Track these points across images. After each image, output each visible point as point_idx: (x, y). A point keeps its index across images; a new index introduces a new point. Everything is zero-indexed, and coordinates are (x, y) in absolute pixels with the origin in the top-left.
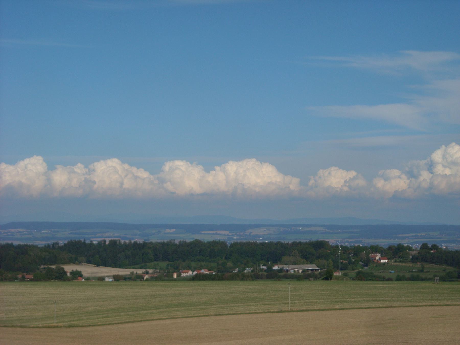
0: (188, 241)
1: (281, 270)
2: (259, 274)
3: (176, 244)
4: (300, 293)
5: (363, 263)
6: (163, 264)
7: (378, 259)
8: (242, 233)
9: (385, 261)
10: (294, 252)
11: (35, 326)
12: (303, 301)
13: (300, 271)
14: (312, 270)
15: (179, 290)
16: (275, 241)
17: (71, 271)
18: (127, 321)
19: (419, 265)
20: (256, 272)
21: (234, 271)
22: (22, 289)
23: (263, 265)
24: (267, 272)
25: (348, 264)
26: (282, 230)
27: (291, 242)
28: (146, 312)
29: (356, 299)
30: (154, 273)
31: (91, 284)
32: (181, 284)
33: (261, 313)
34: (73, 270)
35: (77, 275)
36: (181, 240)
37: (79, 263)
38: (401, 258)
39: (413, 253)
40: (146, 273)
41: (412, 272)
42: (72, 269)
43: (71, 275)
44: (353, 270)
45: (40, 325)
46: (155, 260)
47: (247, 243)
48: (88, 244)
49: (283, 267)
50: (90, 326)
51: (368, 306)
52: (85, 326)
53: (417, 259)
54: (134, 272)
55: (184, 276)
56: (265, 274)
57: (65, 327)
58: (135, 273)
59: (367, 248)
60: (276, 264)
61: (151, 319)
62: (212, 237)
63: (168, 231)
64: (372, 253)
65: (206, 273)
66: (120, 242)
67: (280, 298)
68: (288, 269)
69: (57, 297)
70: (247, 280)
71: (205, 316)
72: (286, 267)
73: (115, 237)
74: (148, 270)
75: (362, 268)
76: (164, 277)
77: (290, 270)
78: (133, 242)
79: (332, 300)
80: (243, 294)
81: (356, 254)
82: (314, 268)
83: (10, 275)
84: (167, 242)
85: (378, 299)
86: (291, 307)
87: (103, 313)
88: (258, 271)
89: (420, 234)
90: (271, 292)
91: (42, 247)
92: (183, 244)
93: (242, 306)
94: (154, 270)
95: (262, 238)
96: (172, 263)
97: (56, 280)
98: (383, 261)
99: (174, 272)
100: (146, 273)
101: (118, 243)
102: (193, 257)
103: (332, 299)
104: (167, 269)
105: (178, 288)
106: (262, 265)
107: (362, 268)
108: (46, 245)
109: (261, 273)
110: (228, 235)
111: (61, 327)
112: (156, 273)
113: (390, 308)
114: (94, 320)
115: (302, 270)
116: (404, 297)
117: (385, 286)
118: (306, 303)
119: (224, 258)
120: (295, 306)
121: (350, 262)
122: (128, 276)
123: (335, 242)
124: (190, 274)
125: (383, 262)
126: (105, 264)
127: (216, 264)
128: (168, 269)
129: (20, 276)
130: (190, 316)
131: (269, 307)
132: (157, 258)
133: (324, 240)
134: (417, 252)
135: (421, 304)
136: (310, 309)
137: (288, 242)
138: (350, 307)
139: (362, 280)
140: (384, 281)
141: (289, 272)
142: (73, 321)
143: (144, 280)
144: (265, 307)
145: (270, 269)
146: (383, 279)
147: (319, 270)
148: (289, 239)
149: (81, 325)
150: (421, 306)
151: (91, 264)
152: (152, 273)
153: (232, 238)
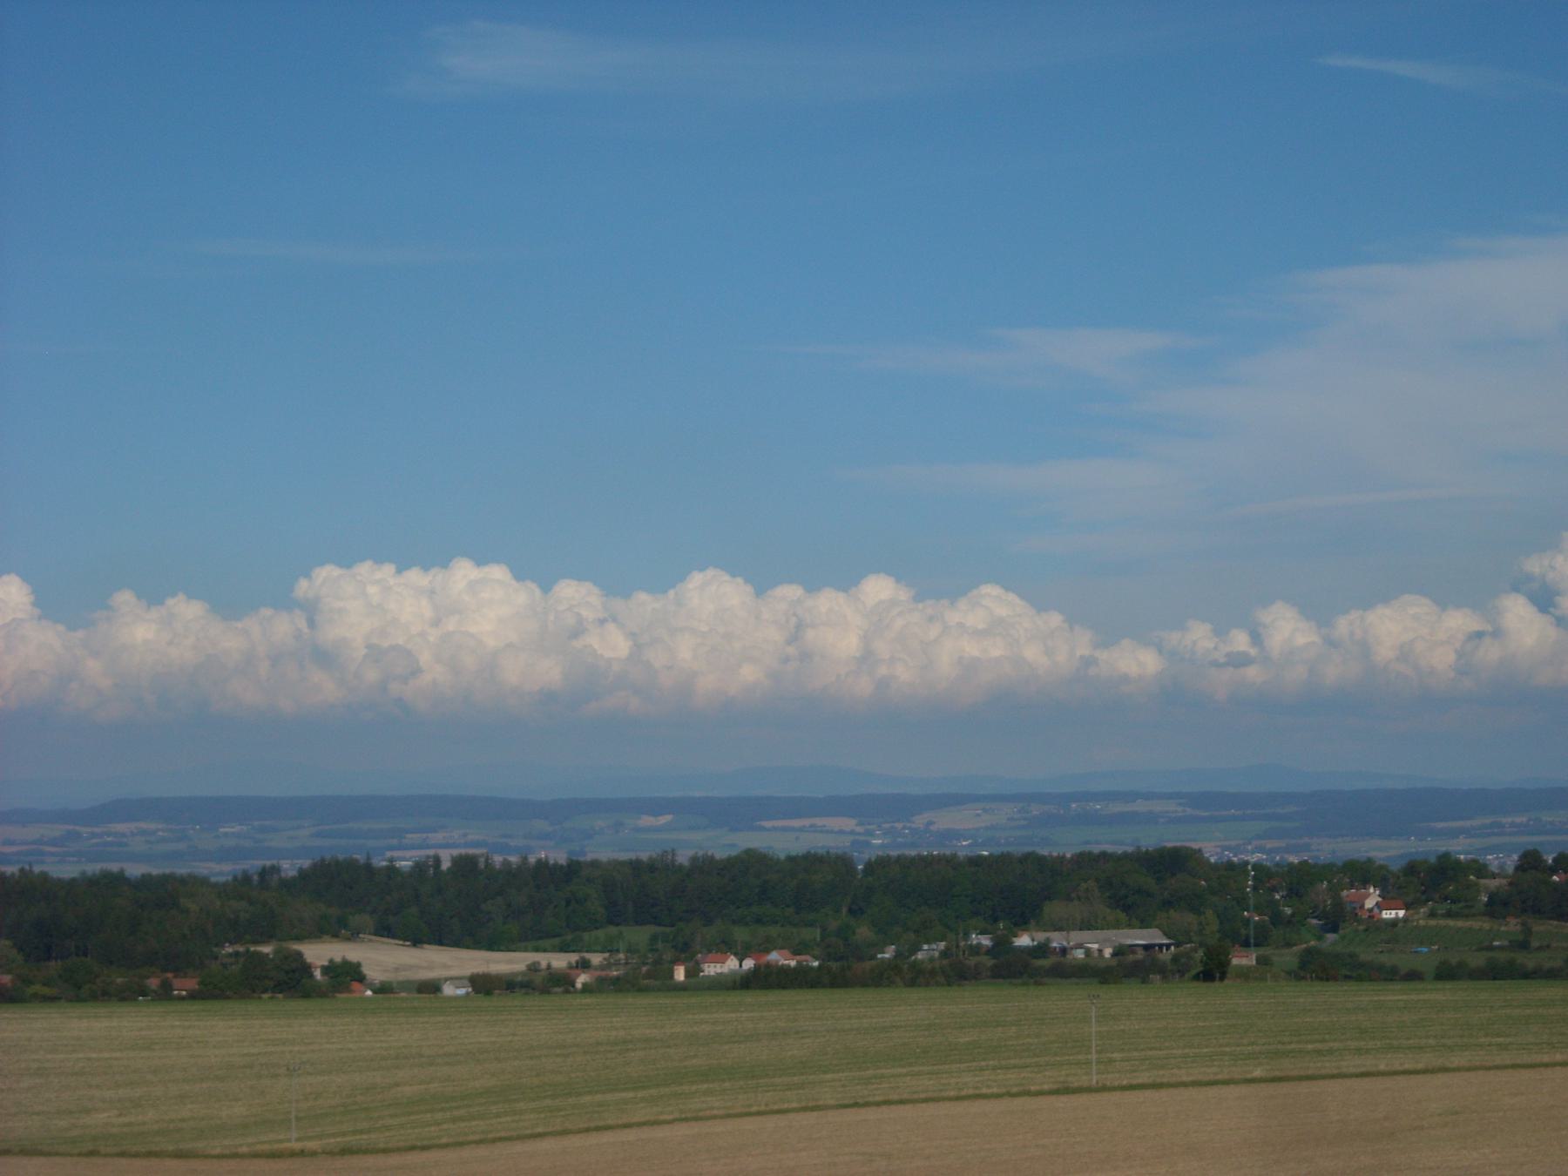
0: (720, 854)
1: (1042, 950)
2: (967, 961)
3: (681, 866)
4: (1122, 1027)
5: (1320, 920)
6: (640, 935)
7: (1371, 906)
8: (899, 825)
9: (1397, 913)
10: (1084, 885)
11: (227, 1152)
12: (1136, 1054)
13: (1108, 952)
14: (1147, 947)
15: (707, 1022)
16: (1018, 850)
17: (326, 963)
18: (540, 1130)
19: (1512, 925)
20: (957, 955)
21: (879, 956)
22: (173, 1027)
23: (978, 931)
24: (994, 958)
25: (1271, 926)
26: (1035, 813)
27: (1074, 852)
28: (599, 1097)
29: (1319, 1046)
30: (606, 966)
31: (405, 1005)
32: (712, 1000)
33: (998, 1096)
34: (331, 961)
35: (346, 976)
36: (696, 853)
37: (353, 936)
38: (1451, 903)
39: (1493, 884)
40: (580, 965)
41: (1491, 948)
42: (329, 957)
43: (326, 978)
44: (1289, 945)
45: (244, 1149)
46: (611, 922)
47: (921, 858)
48: (381, 869)
49: (1048, 940)
50: (412, 1148)
51: (1363, 1070)
52: (398, 1150)
53: (1505, 904)
54: (539, 963)
55: (712, 973)
56: (989, 962)
57: (330, 1153)
58: (544, 965)
59: (1335, 869)
60: (1023, 930)
61: (620, 1122)
62: (797, 838)
63: (647, 821)
64: (1352, 887)
65: (787, 962)
66: (490, 861)
67: (1056, 1045)
68: (1065, 943)
69: (291, 1052)
70: (927, 985)
71: (805, 1109)
72: (1057, 940)
73: (466, 845)
74: (587, 956)
75: (1320, 938)
76: (643, 979)
77: (1072, 948)
78: (532, 860)
79: (1238, 1049)
80: (926, 1033)
81: (1294, 892)
82: (1153, 942)
83: (119, 980)
84: (650, 858)
85: (1395, 1043)
86: (1098, 1073)
87: (454, 1104)
88: (964, 951)
89: (1510, 820)
90: (1024, 1025)
91: (225, 884)
92: (704, 866)
93: (928, 1074)
94: (607, 955)
95: (970, 841)
96: (668, 930)
97: (280, 996)
98: (1391, 914)
99: (676, 961)
100: (580, 965)
101: (482, 865)
102: (739, 907)
103: (1238, 1046)
104: (652, 950)
105: (702, 1016)
106: (977, 934)
107: (1320, 938)
108: (239, 877)
109: (973, 961)
110: (852, 832)
111: (313, 1154)
112: (615, 964)
113: (1440, 1075)
114: (426, 1129)
115: (1114, 948)
116: (1486, 1035)
117: (1414, 997)
118: (1147, 1062)
119: (844, 910)
120: (1113, 1072)
121: (1277, 919)
122: (520, 979)
123: (1219, 850)
124: (732, 967)
125: (1388, 916)
126: (440, 936)
127: (818, 931)
128: (657, 950)
129: (153, 983)
130: (755, 1109)
131: (1022, 1075)
132: (615, 917)
133: (1187, 844)
134: (1504, 882)
135: (1546, 1059)
136: (1165, 1080)
137: (1061, 854)
138: (1302, 1073)
139: (1327, 980)
140: (1395, 980)
141: (1068, 956)
142: (354, 1133)
143: (576, 991)
144: (1009, 1076)
145: (1002, 946)
146: (1391, 975)
147: (1173, 948)
148: (1065, 843)
149: (382, 1146)
150: (1546, 1065)
151: (394, 937)
152: (602, 967)
153: (868, 844)
